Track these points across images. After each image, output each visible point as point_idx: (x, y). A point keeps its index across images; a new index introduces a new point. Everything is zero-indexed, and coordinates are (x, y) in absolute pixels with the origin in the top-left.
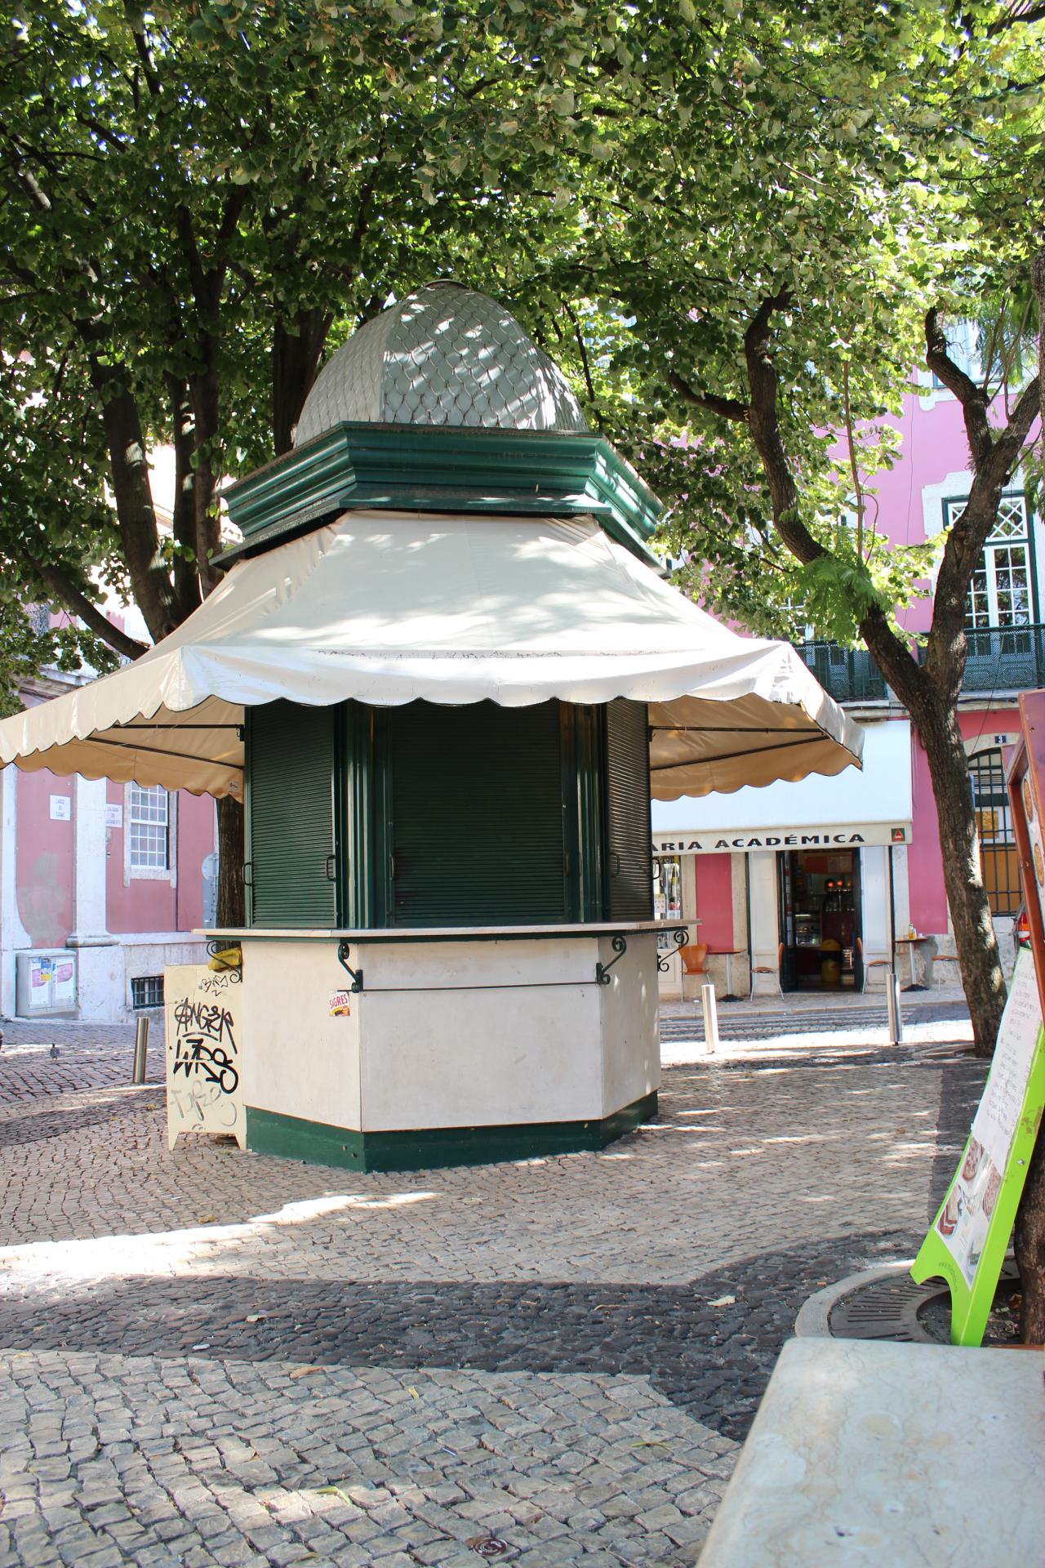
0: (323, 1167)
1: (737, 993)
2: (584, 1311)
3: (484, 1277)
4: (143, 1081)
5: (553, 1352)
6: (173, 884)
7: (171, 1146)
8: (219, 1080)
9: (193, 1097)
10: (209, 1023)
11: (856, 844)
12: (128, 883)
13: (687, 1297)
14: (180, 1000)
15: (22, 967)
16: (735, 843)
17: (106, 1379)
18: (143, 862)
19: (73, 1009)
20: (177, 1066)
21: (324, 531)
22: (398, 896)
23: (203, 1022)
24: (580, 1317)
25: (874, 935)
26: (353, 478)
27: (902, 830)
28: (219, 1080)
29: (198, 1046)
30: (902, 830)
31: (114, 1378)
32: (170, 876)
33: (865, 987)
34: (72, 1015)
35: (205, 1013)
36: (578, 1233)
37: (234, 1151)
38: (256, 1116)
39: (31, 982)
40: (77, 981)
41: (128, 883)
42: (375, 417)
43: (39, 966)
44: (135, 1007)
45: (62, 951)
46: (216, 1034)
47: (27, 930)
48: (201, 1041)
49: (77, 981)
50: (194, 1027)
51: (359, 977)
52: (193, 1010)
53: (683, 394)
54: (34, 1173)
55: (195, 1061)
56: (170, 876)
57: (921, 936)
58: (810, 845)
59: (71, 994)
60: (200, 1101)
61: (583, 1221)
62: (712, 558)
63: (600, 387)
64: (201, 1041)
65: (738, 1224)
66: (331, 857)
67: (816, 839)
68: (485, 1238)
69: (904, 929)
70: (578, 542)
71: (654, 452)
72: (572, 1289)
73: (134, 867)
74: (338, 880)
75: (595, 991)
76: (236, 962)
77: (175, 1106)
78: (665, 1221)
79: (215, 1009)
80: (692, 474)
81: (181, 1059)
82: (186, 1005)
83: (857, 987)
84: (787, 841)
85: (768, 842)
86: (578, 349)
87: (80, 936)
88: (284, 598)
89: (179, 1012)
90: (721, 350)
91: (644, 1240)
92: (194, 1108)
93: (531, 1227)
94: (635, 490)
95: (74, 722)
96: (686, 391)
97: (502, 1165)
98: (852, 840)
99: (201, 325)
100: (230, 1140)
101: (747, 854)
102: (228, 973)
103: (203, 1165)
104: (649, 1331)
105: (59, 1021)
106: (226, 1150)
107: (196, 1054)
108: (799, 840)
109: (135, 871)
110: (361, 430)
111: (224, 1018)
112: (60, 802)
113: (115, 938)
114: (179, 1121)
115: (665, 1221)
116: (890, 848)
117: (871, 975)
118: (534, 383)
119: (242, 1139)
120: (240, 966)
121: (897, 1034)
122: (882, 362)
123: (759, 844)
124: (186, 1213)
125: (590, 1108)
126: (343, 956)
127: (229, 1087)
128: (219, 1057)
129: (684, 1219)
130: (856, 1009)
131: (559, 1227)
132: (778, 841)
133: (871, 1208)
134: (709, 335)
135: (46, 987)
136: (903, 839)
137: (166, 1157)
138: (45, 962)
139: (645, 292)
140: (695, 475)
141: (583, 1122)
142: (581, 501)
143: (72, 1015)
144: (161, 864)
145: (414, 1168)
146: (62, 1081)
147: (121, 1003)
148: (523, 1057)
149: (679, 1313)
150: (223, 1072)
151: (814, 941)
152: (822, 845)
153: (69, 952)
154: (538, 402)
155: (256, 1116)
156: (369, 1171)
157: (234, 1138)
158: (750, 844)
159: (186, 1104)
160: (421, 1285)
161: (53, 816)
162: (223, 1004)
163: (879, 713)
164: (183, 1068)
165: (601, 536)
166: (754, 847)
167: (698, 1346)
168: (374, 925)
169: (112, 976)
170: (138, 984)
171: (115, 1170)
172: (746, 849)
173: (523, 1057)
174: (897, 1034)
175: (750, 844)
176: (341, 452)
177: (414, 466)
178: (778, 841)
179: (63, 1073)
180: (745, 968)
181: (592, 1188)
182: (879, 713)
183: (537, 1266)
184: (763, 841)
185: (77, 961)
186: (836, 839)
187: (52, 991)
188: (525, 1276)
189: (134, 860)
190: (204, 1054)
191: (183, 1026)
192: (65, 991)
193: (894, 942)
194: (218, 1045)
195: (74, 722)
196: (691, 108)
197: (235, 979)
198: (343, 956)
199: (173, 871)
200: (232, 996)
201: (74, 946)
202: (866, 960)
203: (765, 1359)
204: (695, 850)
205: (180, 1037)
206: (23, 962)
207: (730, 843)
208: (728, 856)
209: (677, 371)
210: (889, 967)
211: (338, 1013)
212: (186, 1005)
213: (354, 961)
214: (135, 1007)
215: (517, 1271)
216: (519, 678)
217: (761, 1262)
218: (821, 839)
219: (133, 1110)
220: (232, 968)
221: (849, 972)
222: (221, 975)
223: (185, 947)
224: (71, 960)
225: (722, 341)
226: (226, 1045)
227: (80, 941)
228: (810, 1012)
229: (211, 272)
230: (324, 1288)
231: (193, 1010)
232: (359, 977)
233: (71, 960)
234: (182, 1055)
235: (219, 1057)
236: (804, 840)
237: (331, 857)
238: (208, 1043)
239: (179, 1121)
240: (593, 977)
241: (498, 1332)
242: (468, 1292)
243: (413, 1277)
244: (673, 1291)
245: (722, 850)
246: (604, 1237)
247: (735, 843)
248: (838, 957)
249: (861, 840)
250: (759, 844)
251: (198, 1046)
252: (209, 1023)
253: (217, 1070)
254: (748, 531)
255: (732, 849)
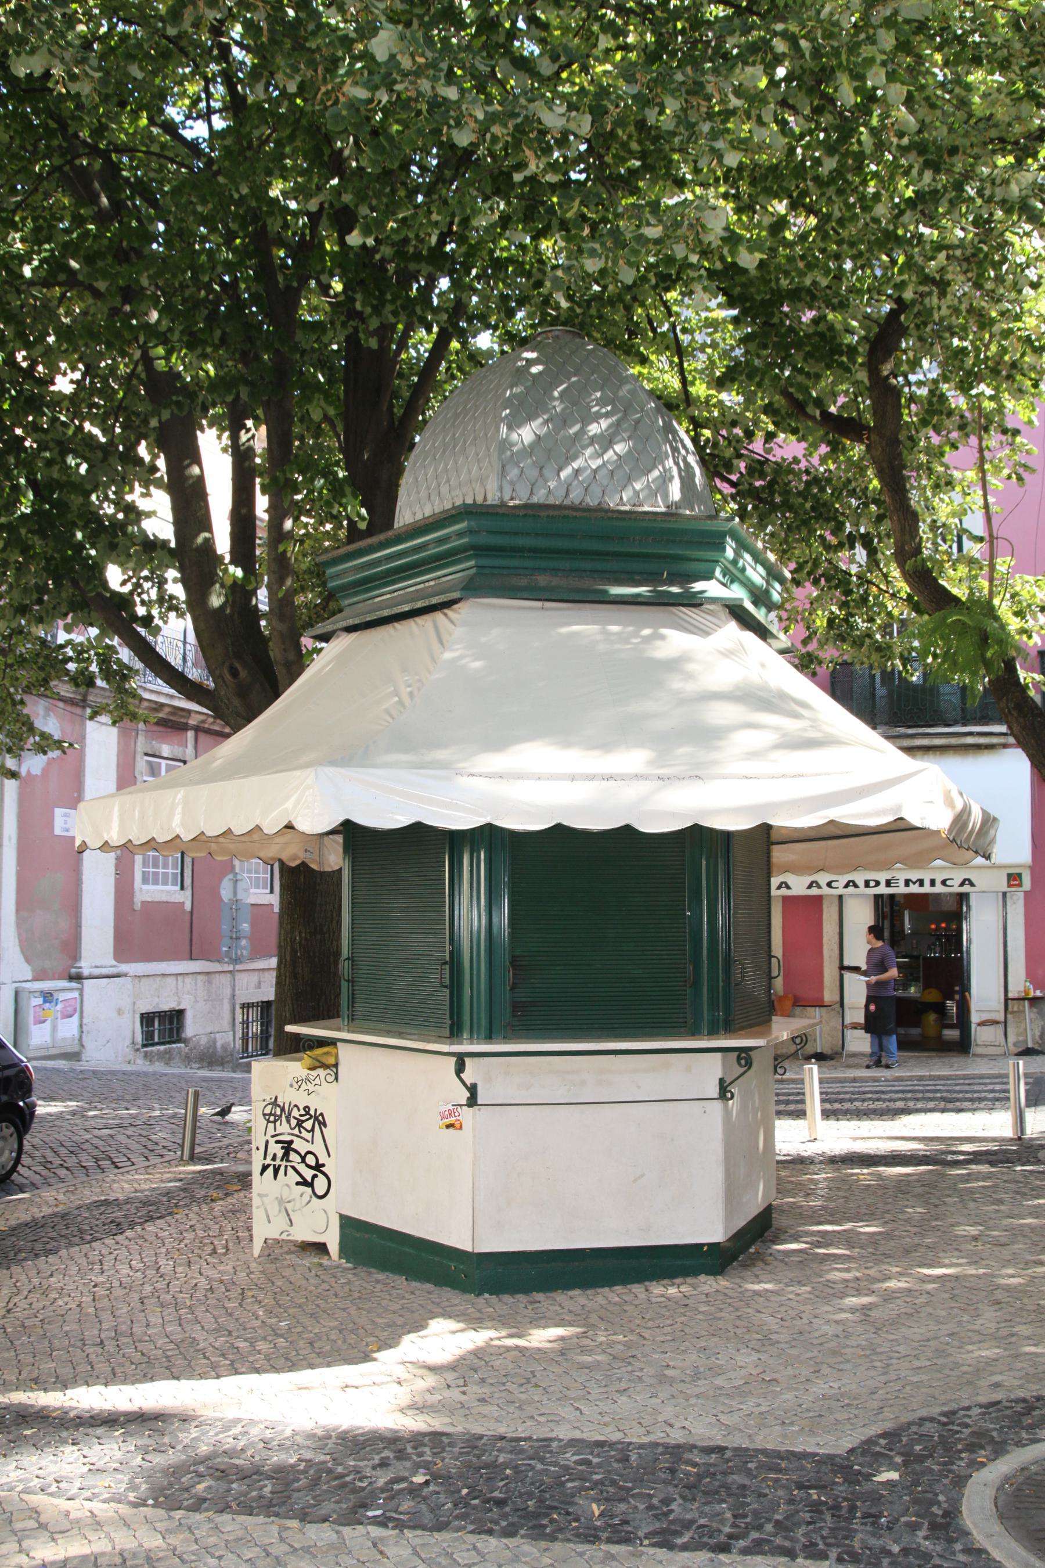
0: (429, 1286)
1: (827, 1051)
2: (747, 1482)
3: (636, 1436)
4: (193, 1158)
5: (727, 1530)
6: (188, 907)
7: (256, 1254)
8: (311, 1185)
9: (281, 1201)
10: (300, 1124)
11: (966, 889)
12: (138, 906)
13: (846, 1468)
14: (269, 1097)
15: (23, 1002)
16: (829, 885)
17: (296, 1550)
18: (156, 882)
19: (76, 1049)
20: (265, 1168)
21: (439, 616)
22: (516, 1006)
23: (294, 1122)
24: (744, 1487)
25: (985, 991)
26: (472, 563)
27: (1020, 875)
28: (311, 1185)
29: (288, 1147)
30: (1020, 875)
31: (302, 1548)
32: (185, 898)
33: (974, 1049)
34: (75, 1056)
35: (295, 1113)
36: (719, 1381)
37: (325, 1261)
38: (349, 1225)
39: (31, 1019)
40: (81, 1017)
41: (138, 906)
42: (492, 499)
43: (40, 1001)
44: (144, 1046)
45: (64, 984)
46: (308, 1136)
47: (28, 960)
48: (291, 1142)
49: (81, 1017)
50: (283, 1127)
51: (473, 1089)
52: (283, 1110)
53: (795, 411)
54: (116, 1283)
55: (284, 1163)
56: (185, 898)
57: (1038, 993)
58: (915, 889)
59: (75, 1032)
60: (289, 1206)
61: (720, 1366)
62: (816, 582)
63: (693, 383)
64: (291, 1142)
65: (883, 1379)
66: (445, 963)
67: (921, 882)
68: (623, 1385)
69: (1019, 983)
70: (708, 634)
71: (758, 467)
72: (728, 1454)
73: (145, 887)
74: (451, 987)
75: (718, 1105)
76: (332, 1061)
77: (262, 1210)
78: (805, 1372)
79: (307, 1109)
80: (800, 494)
81: (268, 1161)
82: (275, 1103)
83: (963, 1046)
84: (888, 883)
85: (867, 884)
86: (673, 346)
87: (86, 966)
88: (407, 700)
89: (267, 1111)
90: (841, 365)
91: (789, 1396)
92: (280, 1212)
93: (668, 1372)
94: (763, 565)
95: (177, 820)
96: (799, 407)
97: (618, 1289)
98: (962, 884)
99: (277, 345)
100: (321, 1248)
101: (841, 897)
102: (322, 1072)
103: (297, 1278)
104: (816, 1507)
105: (62, 1064)
106: (316, 1260)
107: (286, 1156)
108: (902, 883)
109: (146, 892)
110: (482, 514)
111: (316, 1119)
112: (66, 815)
113: (124, 968)
114: (266, 1227)
115: (805, 1372)
116: (1004, 894)
117: (982, 1036)
118: (660, 459)
119: (334, 1248)
120: (336, 1065)
121: (1020, 1121)
122: (1019, 377)
123: (856, 886)
124: (301, 1343)
125: (713, 1231)
126: (460, 1069)
127: (320, 1193)
128: (310, 1160)
129: (825, 1370)
130: (965, 1077)
131: (696, 1376)
132: (878, 883)
133: (1019, 1365)
134: (825, 346)
135: (47, 1025)
136: (1020, 885)
137: (253, 1266)
138: (48, 996)
139: (755, 298)
140: (804, 495)
141: (702, 1245)
142: (711, 588)
143: (75, 1056)
144: (174, 884)
145: (527, 1290)
146: (96, 1153)
147: (128, 1042)
148: (642, 1176)
149: (841, 1489)
150: (315, 1176)
151: (912, 990)
152: (927, 889)
153: (74, 985)
154: (665, 479)
155: (349, 1225)
156: (479, 1294)
157: (324, 1245)
158: (847, 886)
159: (274, 1209)
160: (573, 1443)
161: (58, 831)
162: (316, 1104)
163: (995, 740)
164: (271, 1170)
165: (733, 625)
166: (851, 889)
167: (869, 1528)
168: (489, 1037)
169: (120, 1012)
170: (147, 1019)
171: (203, 1283)
172: (841, 891)
173: (642, 1176)
174: (1020, 1121)
175: (847, 886)
176: (460, 534)
177: (534, 550)
178: (878, 883)
179: (95, 1141)
180: (836, 1023)
181: (720, 1324)
182: (995, 740)
183: (687, 1424)
184: (861, 883)
185: (81, 995)
186: (944, 883)
187: (54, 1028)
188: (677, 1437)
189: (145, 880)
190: (293, 1156)
191: (271, 1125)
192: (68, 1029)
193: (1007, 1000)
194: (309, 1147)
195: (177, 820)
196: (837, 158)
197: (331, 1079)
198: (460, 1069)
199: (188, 892)
200: (324, 1096)
201: (78, 978)
202: (975, 1018)
203: (938, 1548)
204: (784, 891)
205: (268, 1137)
206: (23, 996)
207: (823, 884)
208: (819, 899)
209: (791, 390)
210: (1001, 1027)
211: (449, 1126)
212: (275, 1103)
213: (468, 1076)
214: (144, 1046)
215: (668, 1429)
216: (664, 807)
217: (914, 1428)
218: (927, 883)
219: (194, 1199)
220: (325, 1066)
221: (952, 1026)
222: (314, 1073)
223: (200, 977)
224: (76, 994)
225: (841, 354)
226: (318, 1148)
227: (86, 972)
228: (910, 1078)
229: (288, 287)
230: (473, 1442)
231: (283, 1110)
232: (473, 1089)
233: (76, 994)
234: (270, 1157)
235: (310, 1160)
236: (907, 882)
237: (445, 963)
238: (298, 1145)
239: (266, 1227)
240: (714, 1092)
241: (667, 1501)
242: (622, 1451)
243: (564, 1433)
244: (830, 1459)
245: (814, 891)
246: (746, 1388)
247: (829, 885)
248: (940, 1009)
249: (972, 884)
250: (856, 886)
251: (288, 1147)
252: (300, 1124)
253: (308, 1174)
254: (857, 551)
255: (826, 891)
